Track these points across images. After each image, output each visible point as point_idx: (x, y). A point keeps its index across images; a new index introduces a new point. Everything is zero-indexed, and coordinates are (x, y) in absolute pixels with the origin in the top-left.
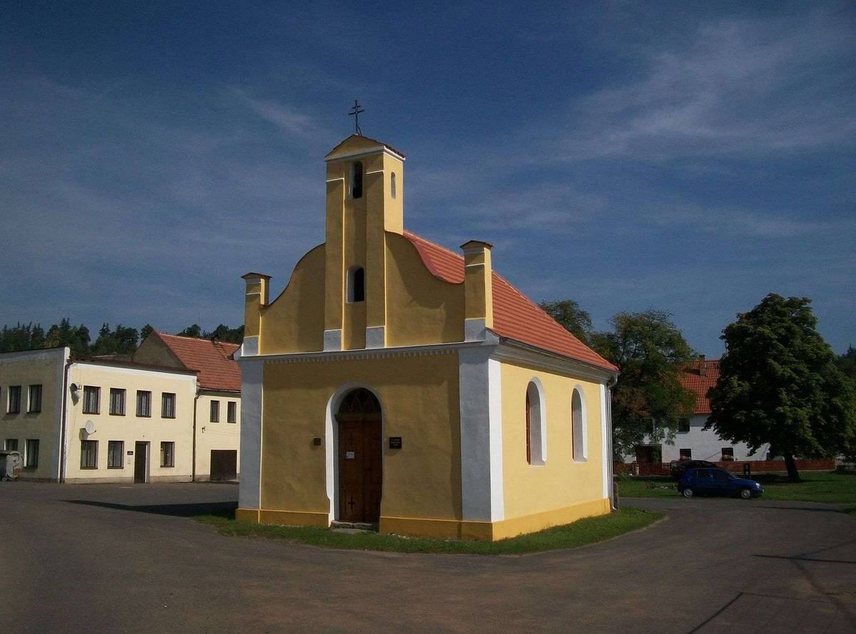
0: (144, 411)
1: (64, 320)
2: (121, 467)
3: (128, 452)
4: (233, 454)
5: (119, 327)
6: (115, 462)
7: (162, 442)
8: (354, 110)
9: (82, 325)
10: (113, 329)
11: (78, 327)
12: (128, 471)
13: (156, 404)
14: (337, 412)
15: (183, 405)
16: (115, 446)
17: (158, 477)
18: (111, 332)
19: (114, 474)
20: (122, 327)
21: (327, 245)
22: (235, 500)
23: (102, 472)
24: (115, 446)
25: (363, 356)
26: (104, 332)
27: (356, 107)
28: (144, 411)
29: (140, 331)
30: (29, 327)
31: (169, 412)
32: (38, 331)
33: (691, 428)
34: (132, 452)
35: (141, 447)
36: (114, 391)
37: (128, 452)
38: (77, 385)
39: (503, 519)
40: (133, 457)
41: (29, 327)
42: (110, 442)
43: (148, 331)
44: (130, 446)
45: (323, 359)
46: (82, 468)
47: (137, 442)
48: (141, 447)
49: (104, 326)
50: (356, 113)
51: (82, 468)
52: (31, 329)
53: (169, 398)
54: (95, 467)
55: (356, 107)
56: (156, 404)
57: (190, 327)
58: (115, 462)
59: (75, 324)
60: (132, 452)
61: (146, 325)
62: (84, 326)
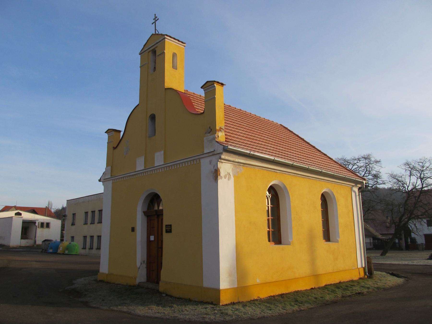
14: (145, 210)
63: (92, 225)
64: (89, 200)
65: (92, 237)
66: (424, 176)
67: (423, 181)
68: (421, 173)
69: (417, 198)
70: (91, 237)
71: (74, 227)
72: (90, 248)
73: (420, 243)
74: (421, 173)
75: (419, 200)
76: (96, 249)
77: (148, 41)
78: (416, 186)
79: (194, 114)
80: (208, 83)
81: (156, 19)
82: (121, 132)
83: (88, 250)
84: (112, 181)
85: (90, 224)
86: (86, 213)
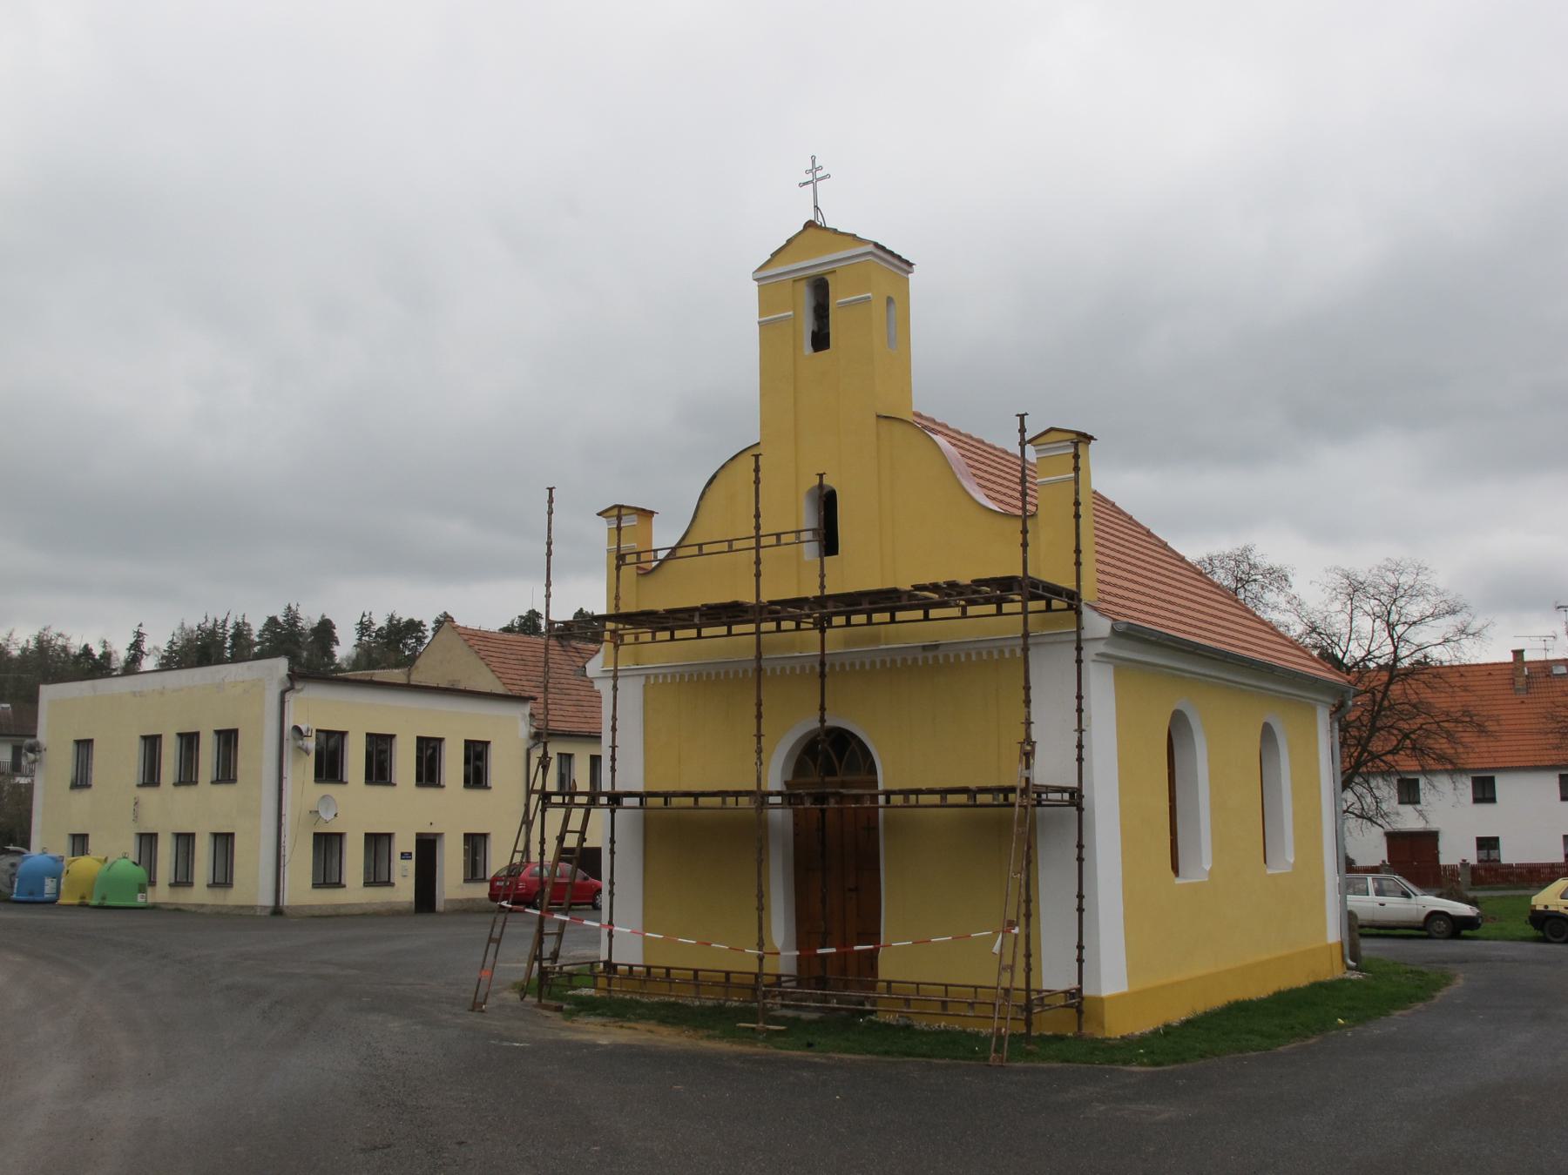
0: (428, 773)
1: (289, 608)
2: (388, 883)
3: (402, 854)
4: (1560, 775)
5: (391, 618)
6: (377, 876)
7: (465, 835)
8: (809, 177)
9: (323, 616)
10: (380, 622)
11: (316, 620)
12: (404, 888)
13: (453, 764)
14: (789, 777)
15: (506, 766)
16: (377, 843)
17: (460, 901)
18: (376, 628)
19: (378, 896)
20: (397, 617)
21: (762, 443)
22: (1480, 852)
23: (354, 891)
24: (377, 843)
25: (788, 668)
26: (364, 627)
27: (815, 169)
28: (428, 773)
29: (429, 625)
30: (225, 621)
31: (476, 776)
32: (240, 633)
33: (487, 896)
34: (410, 854)
35: (427, 847)
36: (423, 743)
37: (402, 854)
38: (304, 728)
39: (1125, 989)
40: (411, 865)
41: (225, 621)
42: (367, 835)
43: (444, 621)
44: (405, 842)
45: (661, 677)
46: (316, 885)
47: (417, 834)
48: (427, 847)
49: (364, 615)
50: (813, 182)
51: (316, 885)
52: (230, 624)
53: (476, 754)
54: (339, 885)
55: (815, 169)
56: (453, 764)
57: (524, 614)
58: (377, 876)
59: (309, 618)
60: (410, 854)
61: (442, 612)
62: (327, 617)
63: (183, 789)
64: (164, 688)
65: (185, 840)
66: (1400, 615)
67: (1395, 636)
68: (1388, 608)
69: (1379, 696)
70: (177, 840)
71: (83, 796)
72: (173, 881)
73: (1456, 861)
74: (1388, 608)
75: (1386, 703)
76: (209, 886)
77: (789, 241)
78: (1371, 649)
79: (991, 510)
80: (1053, 433)
81: (819, 174)
82: (655, 515)
83: (167, 888)
84: (643, 678)
85: (172, 787)
86: (152, 743)
